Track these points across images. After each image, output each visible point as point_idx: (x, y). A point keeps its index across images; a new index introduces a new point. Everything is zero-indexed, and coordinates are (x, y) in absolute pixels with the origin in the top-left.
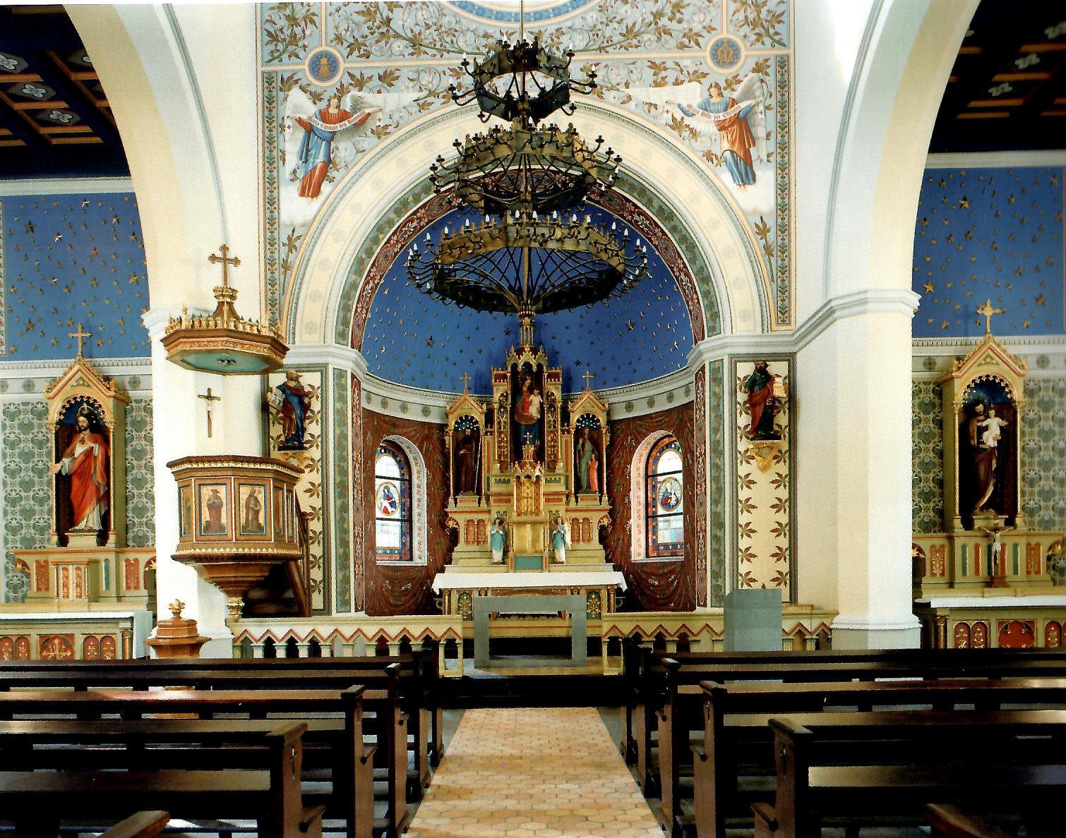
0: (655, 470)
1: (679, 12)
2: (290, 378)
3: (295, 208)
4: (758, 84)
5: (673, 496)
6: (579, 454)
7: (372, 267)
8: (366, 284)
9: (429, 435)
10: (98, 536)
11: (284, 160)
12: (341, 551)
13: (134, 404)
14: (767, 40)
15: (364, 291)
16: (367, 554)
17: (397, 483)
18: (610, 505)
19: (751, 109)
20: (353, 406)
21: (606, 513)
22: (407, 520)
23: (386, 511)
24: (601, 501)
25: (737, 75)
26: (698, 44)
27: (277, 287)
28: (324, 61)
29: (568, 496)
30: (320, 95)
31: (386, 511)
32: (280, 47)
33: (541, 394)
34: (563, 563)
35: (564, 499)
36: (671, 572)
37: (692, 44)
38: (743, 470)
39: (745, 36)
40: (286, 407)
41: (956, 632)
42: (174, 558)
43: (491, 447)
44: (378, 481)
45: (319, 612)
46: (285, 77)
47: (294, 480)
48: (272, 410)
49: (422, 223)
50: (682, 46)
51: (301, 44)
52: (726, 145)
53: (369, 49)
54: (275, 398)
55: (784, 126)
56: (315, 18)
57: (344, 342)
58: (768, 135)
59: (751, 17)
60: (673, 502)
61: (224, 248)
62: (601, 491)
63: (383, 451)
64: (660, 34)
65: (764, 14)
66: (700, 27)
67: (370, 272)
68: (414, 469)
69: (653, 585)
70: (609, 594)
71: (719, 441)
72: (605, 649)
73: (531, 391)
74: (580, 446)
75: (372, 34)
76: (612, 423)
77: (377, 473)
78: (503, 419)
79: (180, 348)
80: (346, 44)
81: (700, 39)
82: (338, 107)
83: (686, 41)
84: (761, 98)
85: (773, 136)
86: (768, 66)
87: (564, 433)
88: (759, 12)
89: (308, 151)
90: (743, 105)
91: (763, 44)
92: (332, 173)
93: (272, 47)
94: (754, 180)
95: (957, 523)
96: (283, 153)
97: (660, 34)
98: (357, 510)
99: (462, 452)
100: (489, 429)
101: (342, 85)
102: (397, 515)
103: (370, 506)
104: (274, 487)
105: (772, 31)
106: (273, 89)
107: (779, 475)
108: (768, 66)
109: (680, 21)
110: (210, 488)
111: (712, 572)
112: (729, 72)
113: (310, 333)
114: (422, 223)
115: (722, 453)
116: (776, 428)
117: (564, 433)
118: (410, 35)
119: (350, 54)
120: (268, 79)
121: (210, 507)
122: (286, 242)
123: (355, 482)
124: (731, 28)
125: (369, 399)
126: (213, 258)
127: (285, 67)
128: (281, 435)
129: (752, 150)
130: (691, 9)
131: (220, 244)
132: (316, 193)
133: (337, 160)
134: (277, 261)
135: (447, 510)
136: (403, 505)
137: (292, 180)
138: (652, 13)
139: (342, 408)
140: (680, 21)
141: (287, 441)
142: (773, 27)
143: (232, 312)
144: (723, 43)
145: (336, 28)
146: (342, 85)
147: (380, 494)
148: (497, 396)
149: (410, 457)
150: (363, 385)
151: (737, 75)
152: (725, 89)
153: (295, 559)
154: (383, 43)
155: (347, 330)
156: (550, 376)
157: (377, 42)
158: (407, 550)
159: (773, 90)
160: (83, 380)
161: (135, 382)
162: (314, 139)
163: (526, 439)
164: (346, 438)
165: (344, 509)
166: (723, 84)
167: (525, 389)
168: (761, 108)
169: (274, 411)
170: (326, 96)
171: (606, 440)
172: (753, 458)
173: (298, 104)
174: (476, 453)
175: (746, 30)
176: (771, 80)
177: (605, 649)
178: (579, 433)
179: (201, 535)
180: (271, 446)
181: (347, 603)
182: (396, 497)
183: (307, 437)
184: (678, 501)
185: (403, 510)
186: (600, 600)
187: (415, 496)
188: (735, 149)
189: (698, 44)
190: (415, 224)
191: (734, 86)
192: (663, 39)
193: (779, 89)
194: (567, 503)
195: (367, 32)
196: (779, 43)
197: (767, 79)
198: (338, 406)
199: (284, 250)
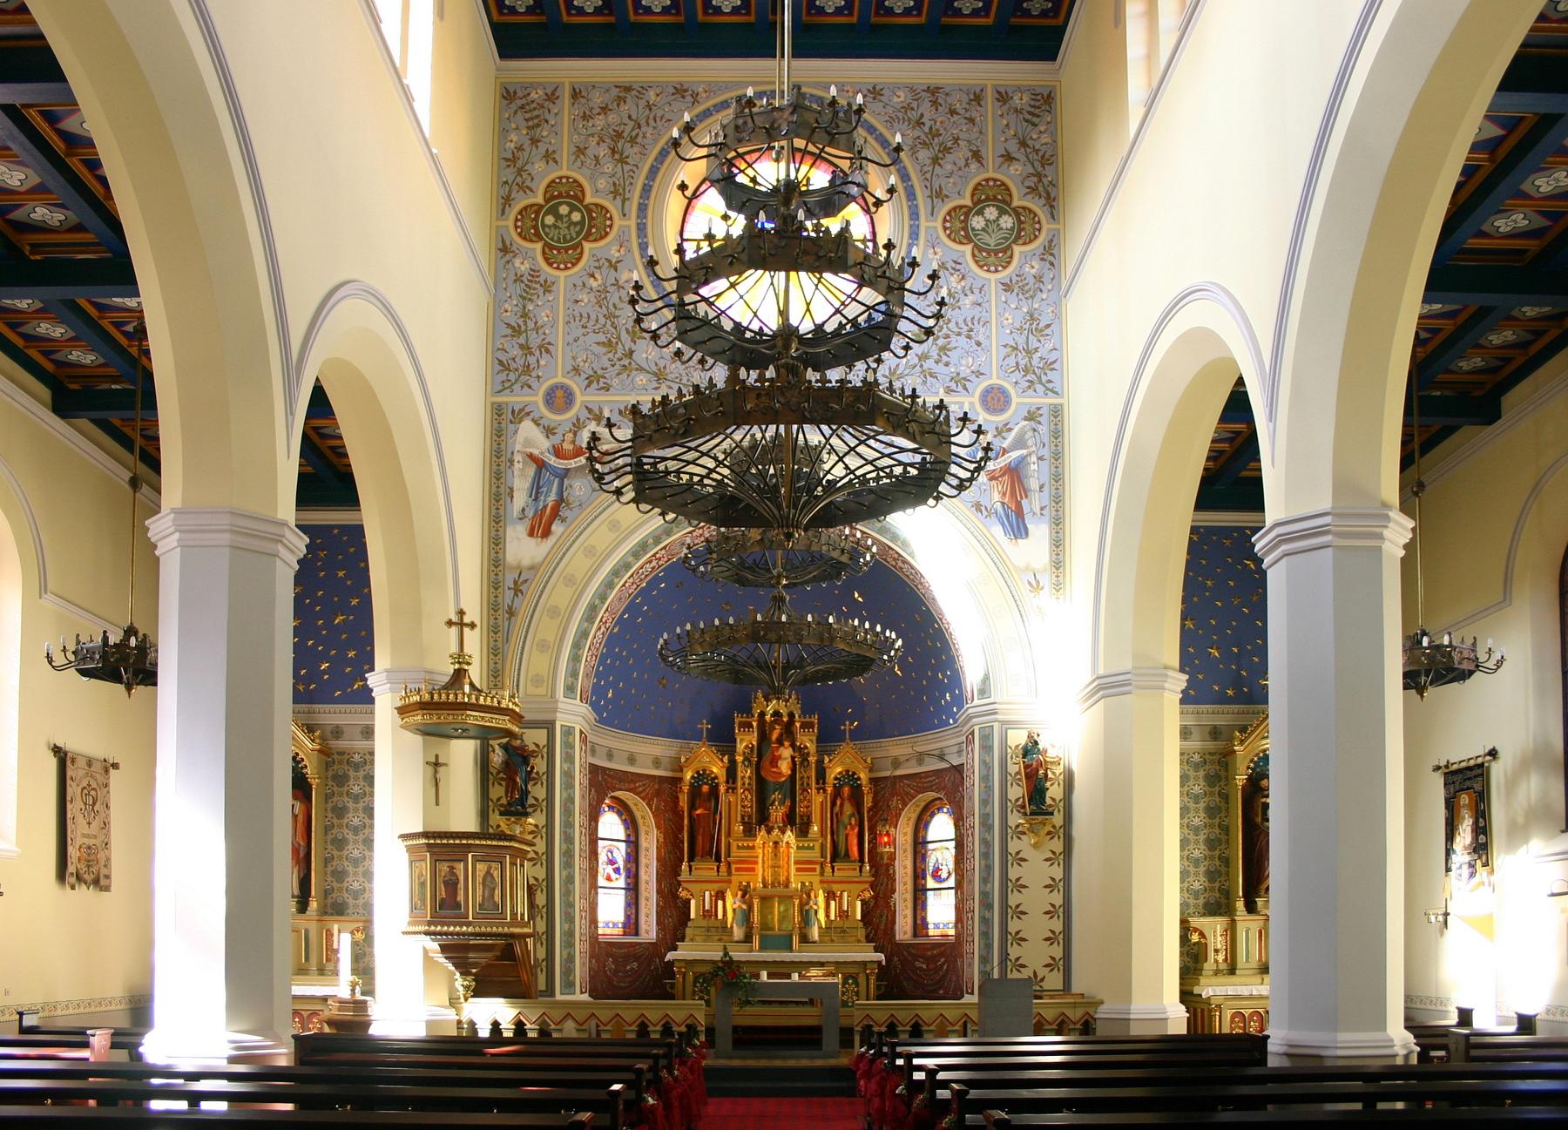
0: (924, 837)
3: (522, 548)
4: (1030, 434)
6: (836, 818)
9: (663, 791)
12: (566, 926)
13: (336, 757)
14: (1039, 388)
17: (623, 846)
19: (1023, 458)
22: (633, 889)
23: (609, 879)
28: (559, 393)
31: (609, 879)
32: (512, 377)
36: (941, 955)
37: (960, 388)
38: (1013, 846)
41: (1232, 1021)
43: (736, 803)
45: (543, 994)
52: (996, 497)
55: (1058, 478)
58: (1041, 487)
59: (1022, 363)
62: (861, 860)
68: (642, 829)
69: (921, 969)
73: (780, 742)
74: (837, 809)
76: (874, 781)
78: (745, 773)
82: (573, 442)
83: (953, 386)
85: (1046, 489)
89: (539, 487)
90: (1015, 454)
92: (564, 512)
93: (503, 376)
95: (1240, 905)
96: (512, 490)
102: (621, 882)
103: (593, 872)
105: (1044, 379)
106: (501, 421)
109: (947, 364)
111: (981, 957)
112: (1000, 419)
116: (1048, 801)
118: (654, 369)
120: (498, 410)
121: (446, 883)
125: (593, 752)
126: (450, 623)
127: (515, 399)
129: (1024, 502)
132: (547, 533)
133: (571, 499)
136: (628, 871)
140: (947, 364)
141: (509, 804)
147: (603, 858)
149: (638, 815)
153: (525, 936)
154: (624, 376)
156: (804, 726)
158: (632, 923)
159: (1046, 440)
162: (546, 475)
165: (569, 880)
167: (774, 737)
168: (1034, 458)
170: (560, 431)
173: (529, 437)
175: (1018, 376)
178: (837, 792)
181: (572, 984)
182: (621, 864)
183: (531, 801)
185: (628, 877)
187: (643, 861)
194: (822, 874)
195: (607, 364)
197: (1040, 428)
198: (565, 766)
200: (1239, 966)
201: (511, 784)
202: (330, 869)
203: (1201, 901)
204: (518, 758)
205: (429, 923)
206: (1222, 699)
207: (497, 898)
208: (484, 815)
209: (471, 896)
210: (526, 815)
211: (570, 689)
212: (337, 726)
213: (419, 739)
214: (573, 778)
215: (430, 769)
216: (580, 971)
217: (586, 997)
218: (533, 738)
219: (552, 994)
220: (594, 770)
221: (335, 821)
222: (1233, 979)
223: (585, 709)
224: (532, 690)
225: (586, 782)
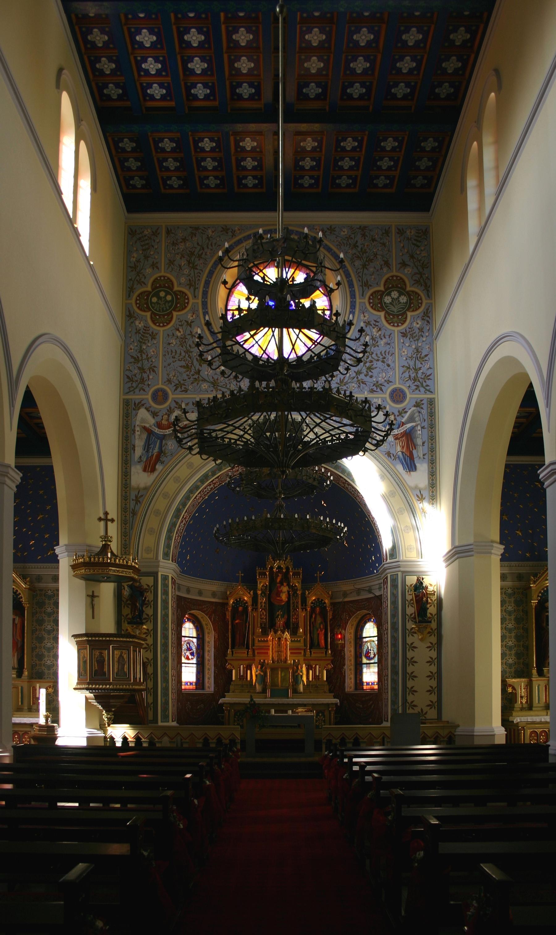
1: (371, 371)
4: (417, 414)
5: (372, 651)
10: (17, 672)
11: (134, 450)
12: (164, 685)
14: (422, 389)
16: (177, 685)
18: (333, 656)
21: (329, 662)
24: (326, 654)
25: (405, 409)
26: (381, 390)
27: (128, 525)
28: (160, 394)
29: (305, 651)
30: (157, 413)
32: (134, 385)
33: (288, 585)
34: (301, 693)
35: (302, 652)
37: (378, 390)
38: (409, 640)
39: (409, 386)
41: (531, 736)
42: (75, 689)
46: (137, 402)
49: (215, 486)
50: (372, 391)
51: (146, 383)
52: (399, 449)
53: (187, 387)
56: (155, 369)
57: (168, 558)
58: (423, 443)
60: (372, 656)
62: (326, 648)
64: (359, 383)
65: (420, 374)
66: (383, 380)
68: (206, 631)
70: (330, 713)
71: (395, 623)
72: (324, 746)
73: (281, 583)
74: (313, 620)
75: (189, 378)
76: (333, 604)
80: (173, 384)
81: (383, 387)
82: (168, 420)
84: (419, 422)
85: (426, 444)
86: (423, 404)
87: (303, 611)
88: (417, 373)
89: (149, 445)
90: (409, 426)
91: (420, 391)
92: (163, 458)
93: (129, 385)
94: (416, 469)
95: (534, 672)
96: (134, 446)
97: (359, 383)
98: (173, 660)
99: (237, 621)
100: (254, 607)
101: (170, 408)
105: (424, 384)
107: (431, 643)
108: (423, 404)
109: (371, 377)
110: (98, 651)
112: (401, 406)
114: (215, 486)
115: (397, 629)
116: (429, 615)
117: (303, 611)
118: (212, 380)
119: (176, 390)
121: (98, 662)
124: (401, 381)
126: (100, 519)
127: (136, 397)
130: (378, 369)
132: (153, 470)
134: (128, 510)
135: (227, 658)
137: (139, 462)
138: (355, 372)
139: (165, 598)
141: (133, 618)
142: (425, 382)
144: (396, 390)
145: (168, 375)
146: (170, 408)
148: (260, 586)
149: (204, 623)
151: (405, 409)
152: (398, 416)
153: (141, 690)
154: (196, 384)
157: (192, 383)
159: (426, 418)
163: (278, 615)
166: (397, 414)
168: (419, 428)
169: (125, 600)
170: (160, 414)
171: (330, 615)
172: (415, 633)
173: (143, 416)
174: (246, 622)
175: (410, 383)
176: (424, 412)
177: (324, 746)
183: (145, 616)
184: (375, 655)
186: (324, 717)
188: (404, 451)
189: (381, 390)
190: (212, 486)
191: (403, 415)
192: (361, 387)
193: (429, 417)
194: (305, 655)
195: (186, 378)
196: (429, 391)
197: (422, 411)
198: (164, 597)
199: (133, 503)
200: (534, 705)
202: (35, 653)
203: (513, 670)
206: (523, 559)
207: (126, 669)
209: (112, 669)
210: (143, 624)
212: (39, 575)
214: (168, 603)
215: (89, 599)
217: (174, 724)
218: (147, 581)
219: (157, 722)
222: (531, 713)
225: (175, 606)
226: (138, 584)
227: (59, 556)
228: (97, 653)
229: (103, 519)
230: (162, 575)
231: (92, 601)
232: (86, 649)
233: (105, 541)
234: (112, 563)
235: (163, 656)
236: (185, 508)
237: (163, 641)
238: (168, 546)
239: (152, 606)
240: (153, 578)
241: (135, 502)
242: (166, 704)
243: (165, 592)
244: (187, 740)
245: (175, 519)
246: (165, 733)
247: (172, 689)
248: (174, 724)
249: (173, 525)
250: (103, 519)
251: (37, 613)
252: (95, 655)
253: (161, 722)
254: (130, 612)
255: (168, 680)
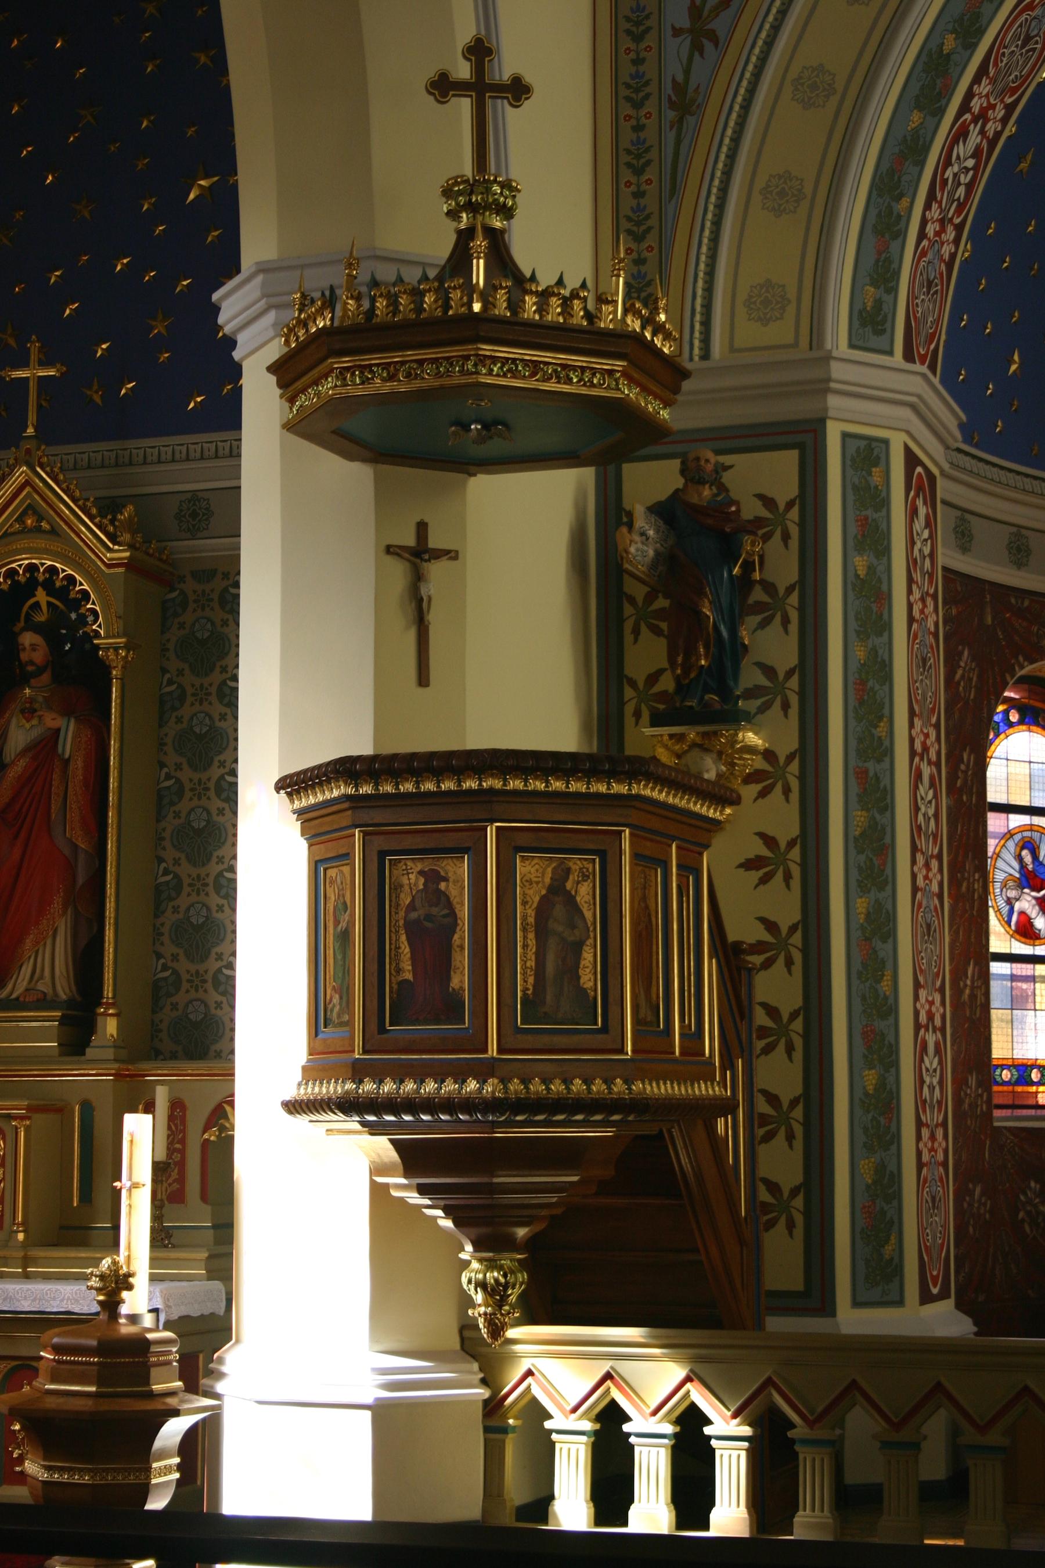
2: (692, 473)
7: (977, 80)
8: (955, 141)
10: (62, 1021)
12: (870, 1078)
15: (948, 163)
16: (960, 1083)
20: (912, 564)
27: (650, 173)
40: (676, 572)
42: (294, 1107)
44: (995, 823)
45: (788, 1303)
47: (699, 834)
48: (631, 587)
54: (642, 546)
57: (881, 342)
61: (480, 51)
63: (1014, 717)
67: (969, 95)
77: (995, 794)
79: (328, 387)
98: (925, 931)
104: (636, 856)
113: (765, 321)
114: (991, 128)
121: (414, 931)
122: (685, 22)
123: (916, 830)
125: (964, 538)
126: (443, 87)
128: (660, 672)
131: (466, 31)
134: (652, 88)
139: (871, 569)
141: (681, 688)
143: (501, 259)
150: (943, 488)
153: (710, 1110)
155: (888, 298)
160: (35, 512)
161: (194, 515)
164: (887, 678)
165: (876, 927)
169: (639, 591)
179: (382, 1030)
180: (629, 709)
181: (894, 1270)
183: (750, 677)
198: (861, 563)
199: (676, 49)
201: (684, 629)
202: (169, 918)
204: (705, 540)
205: (358, 1072)
207: (589, 978)
208: (606, 714)
209: (491, 970)
210: (735, 718)
211: (870, 324)
212: (195, 497)
213: (357, 476)
214: (884, 598)
215: (398, 571)
216: (921, 1223)
217: (944, 1321)
218: (761, 477)
219: (826, 1307)
220: (963, 592)
221: (186, 775)
223: (916, 382)
224: (749, 333)
225: (933, 618)
226: (707, 492)
227: (241, 338)
228: (410, 876)
229: (461, 87)
230: (845, 436)
231: (418, 578)
232: (346, 856)
233: (472, 208)
234: (500, 321)
235: (861, 905)
236: (972, 47)
237: (860, 817)
238: (880, 272)
239: (794, 616)
240: (794, 454)
241: (685, 43)
242: (880, 1193)
243: (869, 536)
244: (994, 1438)
245: (916, 117)
246: (854, 1384)
247: (921, 1104)
248: (944, 1321)
249: (906, 151)
250: (461, 87)
251: (182, 698)
252: (397, 888)
253: (856, 1304)
254: (665, 664)
255: (894, 1050)
